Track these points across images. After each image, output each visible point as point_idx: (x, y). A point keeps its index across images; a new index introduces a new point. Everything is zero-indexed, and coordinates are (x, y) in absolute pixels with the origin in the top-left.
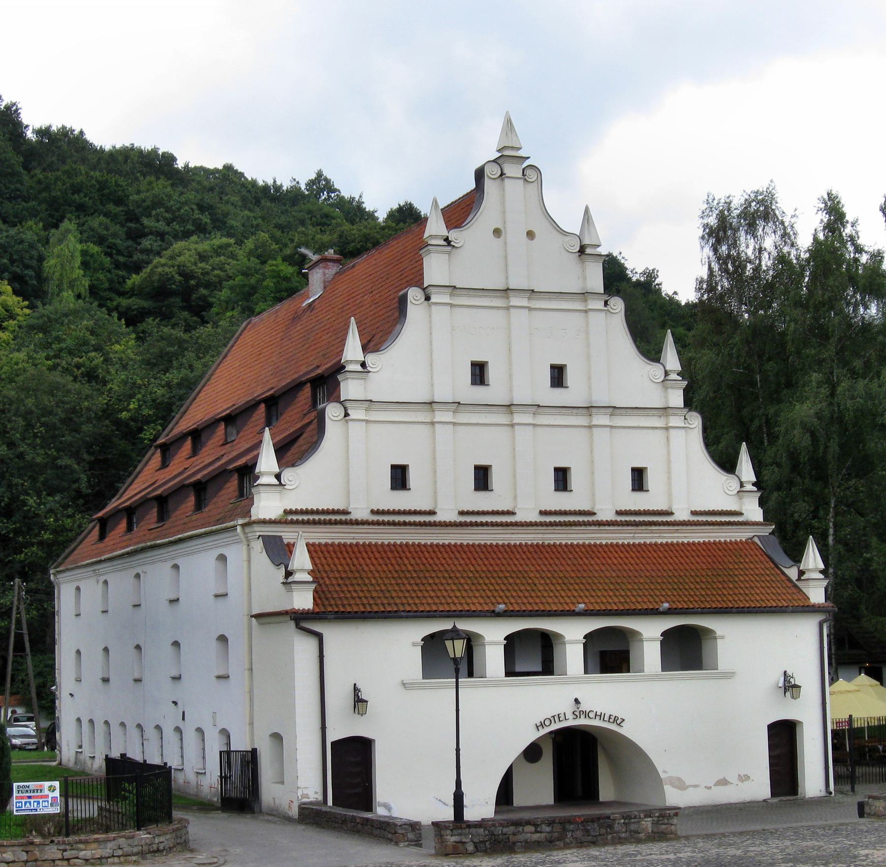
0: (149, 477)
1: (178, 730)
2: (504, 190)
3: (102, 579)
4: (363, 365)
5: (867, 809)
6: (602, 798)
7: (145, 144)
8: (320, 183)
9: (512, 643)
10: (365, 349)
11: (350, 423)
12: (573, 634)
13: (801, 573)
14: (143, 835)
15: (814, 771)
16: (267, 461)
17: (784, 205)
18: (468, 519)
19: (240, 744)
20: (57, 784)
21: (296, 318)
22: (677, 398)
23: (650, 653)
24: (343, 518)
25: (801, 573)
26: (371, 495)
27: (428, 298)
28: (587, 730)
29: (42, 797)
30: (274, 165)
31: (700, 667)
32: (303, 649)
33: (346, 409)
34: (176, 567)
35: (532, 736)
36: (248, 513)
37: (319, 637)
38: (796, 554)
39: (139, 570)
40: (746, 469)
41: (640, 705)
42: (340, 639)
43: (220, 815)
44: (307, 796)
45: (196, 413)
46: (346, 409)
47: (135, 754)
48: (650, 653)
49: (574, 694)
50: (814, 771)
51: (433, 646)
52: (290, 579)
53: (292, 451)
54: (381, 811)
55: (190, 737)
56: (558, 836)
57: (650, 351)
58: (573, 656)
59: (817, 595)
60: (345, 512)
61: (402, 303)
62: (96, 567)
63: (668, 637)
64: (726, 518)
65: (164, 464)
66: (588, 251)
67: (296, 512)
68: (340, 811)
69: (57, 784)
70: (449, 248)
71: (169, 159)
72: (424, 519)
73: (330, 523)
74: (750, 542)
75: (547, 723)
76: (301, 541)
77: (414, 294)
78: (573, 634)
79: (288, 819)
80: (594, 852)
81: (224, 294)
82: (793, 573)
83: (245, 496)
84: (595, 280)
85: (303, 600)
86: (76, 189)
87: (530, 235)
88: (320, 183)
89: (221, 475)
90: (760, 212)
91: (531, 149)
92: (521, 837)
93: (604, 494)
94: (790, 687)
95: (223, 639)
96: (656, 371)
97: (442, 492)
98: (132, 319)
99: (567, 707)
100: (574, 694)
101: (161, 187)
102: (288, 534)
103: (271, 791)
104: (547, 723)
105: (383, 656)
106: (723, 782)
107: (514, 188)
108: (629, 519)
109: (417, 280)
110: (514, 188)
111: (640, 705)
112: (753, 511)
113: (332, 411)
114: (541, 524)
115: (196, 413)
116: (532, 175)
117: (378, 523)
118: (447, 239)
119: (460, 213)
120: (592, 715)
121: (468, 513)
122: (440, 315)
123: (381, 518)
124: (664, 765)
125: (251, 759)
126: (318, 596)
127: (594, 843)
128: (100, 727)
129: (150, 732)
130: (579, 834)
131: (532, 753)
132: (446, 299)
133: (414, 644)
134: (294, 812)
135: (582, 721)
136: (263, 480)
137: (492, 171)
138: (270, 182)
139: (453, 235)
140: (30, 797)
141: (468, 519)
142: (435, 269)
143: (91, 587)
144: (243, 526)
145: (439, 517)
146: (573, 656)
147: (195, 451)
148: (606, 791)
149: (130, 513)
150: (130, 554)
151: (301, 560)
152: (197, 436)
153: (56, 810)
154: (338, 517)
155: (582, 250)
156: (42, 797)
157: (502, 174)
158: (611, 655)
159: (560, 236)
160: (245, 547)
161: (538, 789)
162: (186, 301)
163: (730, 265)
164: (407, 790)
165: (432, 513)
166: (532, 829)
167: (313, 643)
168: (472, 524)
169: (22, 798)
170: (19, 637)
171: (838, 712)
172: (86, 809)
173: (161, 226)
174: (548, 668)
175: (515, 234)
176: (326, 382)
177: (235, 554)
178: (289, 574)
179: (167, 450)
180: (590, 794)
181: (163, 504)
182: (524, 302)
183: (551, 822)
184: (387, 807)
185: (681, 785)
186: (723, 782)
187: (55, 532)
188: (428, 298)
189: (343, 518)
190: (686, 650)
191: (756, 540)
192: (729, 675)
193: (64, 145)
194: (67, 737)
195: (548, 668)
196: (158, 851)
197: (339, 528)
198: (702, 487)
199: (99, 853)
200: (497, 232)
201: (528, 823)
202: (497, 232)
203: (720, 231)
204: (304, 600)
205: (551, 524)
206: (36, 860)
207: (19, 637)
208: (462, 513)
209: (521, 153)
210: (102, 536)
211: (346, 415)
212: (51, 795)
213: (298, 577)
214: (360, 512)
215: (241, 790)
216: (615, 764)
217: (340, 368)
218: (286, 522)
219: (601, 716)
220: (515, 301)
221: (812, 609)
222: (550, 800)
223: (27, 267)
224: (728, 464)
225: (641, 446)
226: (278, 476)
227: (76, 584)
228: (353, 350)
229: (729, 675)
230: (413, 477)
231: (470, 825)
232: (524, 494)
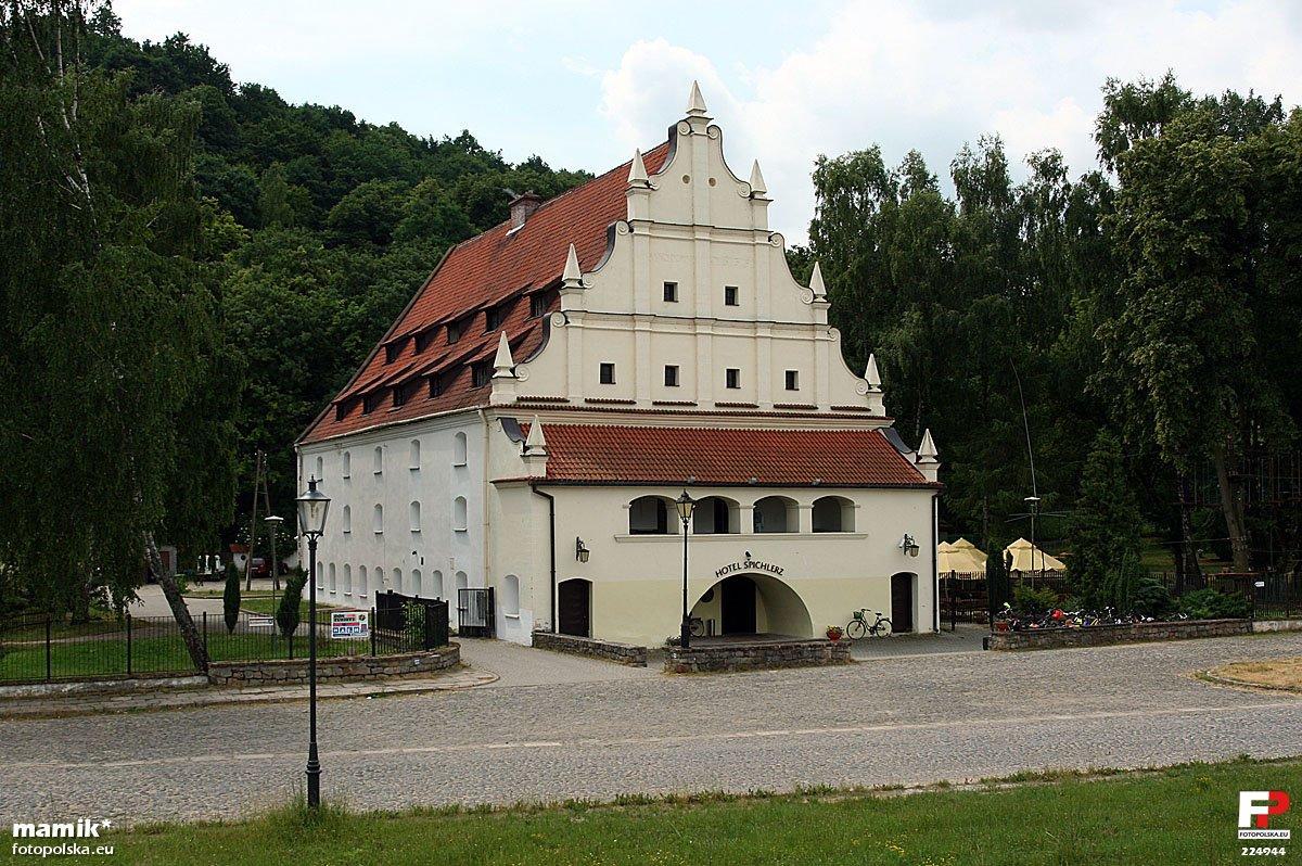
0: (375, 371)
2: (692, 145)
3: (344, 451)
4: (580, 282)
5: (990, 643)
7: (327, 103)
8: (467, 140)
9: (819, 508)
11: (570, 329)
15: (925, 616)
16: (503, 358)
18: (660, 408)
19: (477, 582)
21: (501, 244)
24: (563, 405)
25: (919, 458)
26: (582, 387)
27: (631, 230)
28: (751, 577)
29: (354, 624)
30: (431, 123)
33: (566, 318)
37: (551, 499)
38: (914, 445)
39: (381, 445)
42: (565, 500)
44: (539, 626)
45: (416, 319)
46: (566, 318)
49: (743, 549)
50: (925, 616)
51: (637, 507)
52: (528, 453)
59: (931, 476)
61: (611, 233)
62: (338, 442)
64: (859, 413)
66: (757, 196)
67: (527, 399)
70: (649, 190)
71: (350, 117)
72: (626, 407)
73: (550, 408)
75: (759, 565)
76: (536, 422)
77: (621, 227)
81: (400, 228)
82: (912, 458)
85: (539, 470)
86: (281, 139)
87: (712, 182)
92: (733, 660)
93: (762, 390)
94: (910, 547)
96: (806, 295)
97: (641, 387)
99: (741, 560)
100: (743, 549)
101: (346, 138)
102: (521, 417)
104: (725, 571)
105: (599, 516)
107: (700, 144)
108: (784, 412)
110: (700, 144)
113: (556, 320)
114: (655, 412)
115: (416, 319)
117: (591, 410)
118: (647, 183)
119: (656, 160)
120: (759, 565)
121: (590, 401)
122: (641, 244)
123: (593, 406)
128: (355, 572)
130: (776, 658)
133: (624, 507)
135: (752, 570)
137: (683, 129)
138: (428, 138)
140: (344, 625)
141: (660, 408)
142: (636, 207)
144: (482, 409)
150: (378, 429)
151: (536, 437)
152: (424, 339)
154: (560, 404)
155: (752, 196)
156: (354, 624)
157: (691, 131)
158: (773, 517)
159: (732, 182)
160: (485, 427)
162: (373, 229)
165: (632, 403)
166: (742, 654)
167: (545, 504)
168: (663, 412)
169: (338, 625)
171: (944, 568)
176: (548, 296)
177: (475, 433)
178: (526, 449)
179: (394, 351)
187: (277, 414)
188: (631, 230)
189: (563, 405)
190: (830, 517)
191: (880, 431)
192: (864, 537)
193: (261, 101)
196: (443, 668)
198: (841, 389)
201: (739, 649)
202: (686, 179)
205: (783, 415)
206: (350, 675)
208: (655, 403)
209: (705, 115)
211: (567, 322)
212: (361, 623)
217: (558, 284)
218: (520, 407)
219: (765, 567)
223: (245, 201)
225: (794, 354)
227: (317, 456)
228: (571, 270)
229: (864, 537)
230: (617, 374)
232: (704, 390)
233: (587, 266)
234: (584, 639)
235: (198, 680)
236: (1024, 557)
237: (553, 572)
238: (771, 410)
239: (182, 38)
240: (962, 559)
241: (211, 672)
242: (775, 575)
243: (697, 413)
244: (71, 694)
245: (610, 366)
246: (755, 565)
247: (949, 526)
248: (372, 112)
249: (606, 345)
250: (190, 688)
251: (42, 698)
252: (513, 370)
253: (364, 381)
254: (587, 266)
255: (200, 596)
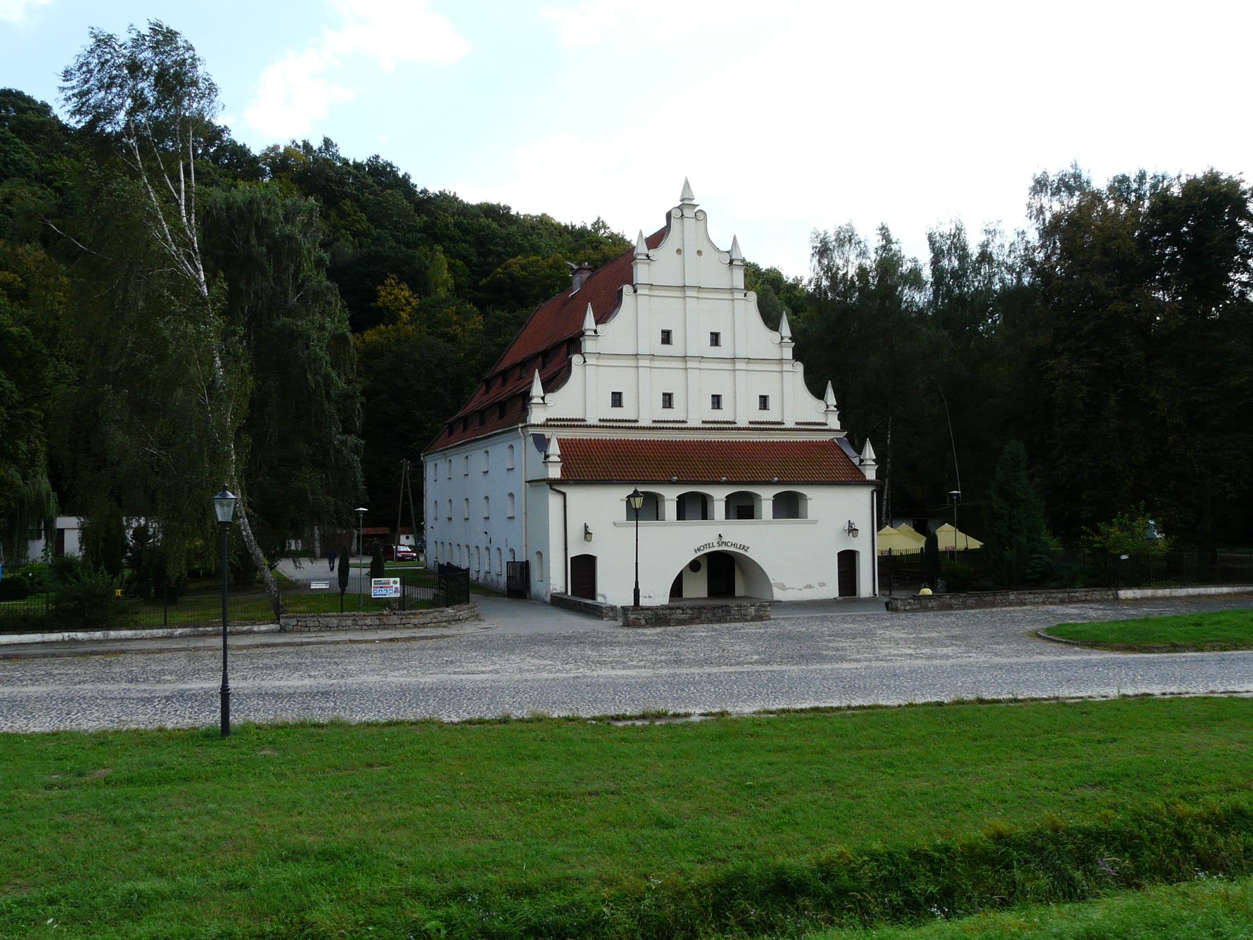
0: (478, 400)
1: (487, 548)
4: (595, 331)
6: (737, 594)
8: (599, 225)
9: (682, 501)
10: (597, 323)
12: (719, 495)
13: (861, 461)
14: (450, 610)
17: (861, 233)
20: (398, 579)
22: (788, 353)
23: (767, 508)
25: (861, 461)
26: (599, 410)
27: (635, 291)
31: (797, 517)
32: (554, 501)
34: (487, 452)
35: (694, 556)
36: (525, 421)
37: (564, 495)
38: (859, 450)
40: (831, 397)
41: (764, 541)
43: (505, 599)
47: (455, 563)
48: (767, 508)
49: (719, 532)
53: (553, 383)
54: (600, 599)
55: (494, 552)
56: (698, 614)
57: (771, 322)
58: (719, 509)
59: (871, 474)
60: (584, 420)
63: (777, 498)
64: (818, 427)
65: (487, 392)
68: (574, 598)
69: (398, 579)
72: (631, 425)
74: (831, 441)
77: (627, 289)
78: (719, 495)
79: (545, 603)
80: (717, 626)
83: (525, 411)
84: (739, 279)
87: (699, 253)
88: (599, 225)
89: (513, 398)
90: (846, 238)
91: (700, 200)
93: (743, 411)
94: (852, 530)
95: (511, 495)
96: (775, 336)
97: (644, 409)
98: (481, 306)
99: (714, 540)
100: (719, 532)
102: (547, 433)
103: (536, 586)
106: (810, 586)
108: (756, 426)
109: (629, 280)
111: (764, 541)
112: (834, 423)
114: (654, 428)
116: (701, 216)
119: (655, 241)
121: (603, 420)
124: (773, 575)
125: (525, 566)
126: (563, 470)
127: (719, 621)
129: (473, 550)
130: (709, 615)
131: (694, 566)
132: (647, 292)
134: (548, 599)
135: (723, 548)
136: (534, 401)
139: (651, 253)
141: (658, 425)
142: (641, 273)
143: (442, 464)
145: (588, 423)
146: (719, 509)
147: (504, 383)
148: (740, 590)
149: (465, 421)
151: (554, 449)
152: (504, 374)
153: (398, 595)
155: (731, 262)
158: (742, 509)
161: (697, 589)
163: (830, 272)
164: (612, 589)
165: (636, 421)
167: (559, 499)
170: (406, 493)
172: (427, 594)
173: (500, 249)
174: (705, 515)
175: (690, 252)
176: (574, 343)
179: (488, 384)
180: (729, 592)
181: (481, 415)
182: (695, 294)
183: (692, 608)
184: (604, 597)
185: (783, 588)
186: (810, 586)
188: (635, 291)
190: (789, 507)
192: (815, 522)
193: (445, 202)
194: (430, 549)
195: (705, 515)
197: (578, 430)
198: (803, 409)
199: (422, 621)
200: (679, 251)
202: (679, 251)
203: (823, 251)
204: (555, 472)
207: (406, 493)
209: (694, 202)
210: (450, 434)
213: (551, 459)
214: (592, 420)
215: (518, 585)
216: (743, 572)
217: (582, 334)
219: (735, 545)
220: (689, 293)
221: (869, 483)
222: (705, 594)
224: (819, 394)
225: (766, 382)
226: (543, 398)
229: (815, 522)
230: (625, 400)
231: (643, 609)
233: (600, 320)
234: (589, 601)
235: (273, 626)
236: (950, 537)
237: (566, 549)
238: (746, 425)
239: (377, 157)
240: (904, 540)
241: (282, 621)
242: (742, 552)
243: (638, 428)
244: (181, 636)
245: (620, 394)
246: (726, 544)
247: (886, 514)
248: (524, 205)
249: (612, 379)
250: (265, 633)
251: (162, 638)
252: (543, 398)
253: (472, 406)
254: (600, 320)
255: (356, 566)
